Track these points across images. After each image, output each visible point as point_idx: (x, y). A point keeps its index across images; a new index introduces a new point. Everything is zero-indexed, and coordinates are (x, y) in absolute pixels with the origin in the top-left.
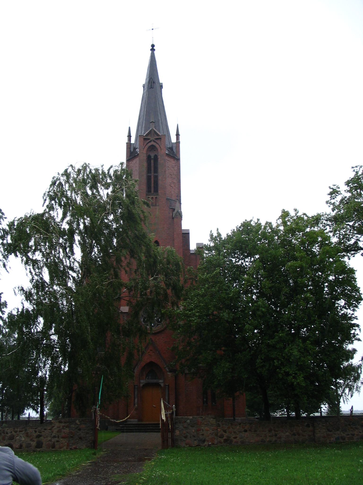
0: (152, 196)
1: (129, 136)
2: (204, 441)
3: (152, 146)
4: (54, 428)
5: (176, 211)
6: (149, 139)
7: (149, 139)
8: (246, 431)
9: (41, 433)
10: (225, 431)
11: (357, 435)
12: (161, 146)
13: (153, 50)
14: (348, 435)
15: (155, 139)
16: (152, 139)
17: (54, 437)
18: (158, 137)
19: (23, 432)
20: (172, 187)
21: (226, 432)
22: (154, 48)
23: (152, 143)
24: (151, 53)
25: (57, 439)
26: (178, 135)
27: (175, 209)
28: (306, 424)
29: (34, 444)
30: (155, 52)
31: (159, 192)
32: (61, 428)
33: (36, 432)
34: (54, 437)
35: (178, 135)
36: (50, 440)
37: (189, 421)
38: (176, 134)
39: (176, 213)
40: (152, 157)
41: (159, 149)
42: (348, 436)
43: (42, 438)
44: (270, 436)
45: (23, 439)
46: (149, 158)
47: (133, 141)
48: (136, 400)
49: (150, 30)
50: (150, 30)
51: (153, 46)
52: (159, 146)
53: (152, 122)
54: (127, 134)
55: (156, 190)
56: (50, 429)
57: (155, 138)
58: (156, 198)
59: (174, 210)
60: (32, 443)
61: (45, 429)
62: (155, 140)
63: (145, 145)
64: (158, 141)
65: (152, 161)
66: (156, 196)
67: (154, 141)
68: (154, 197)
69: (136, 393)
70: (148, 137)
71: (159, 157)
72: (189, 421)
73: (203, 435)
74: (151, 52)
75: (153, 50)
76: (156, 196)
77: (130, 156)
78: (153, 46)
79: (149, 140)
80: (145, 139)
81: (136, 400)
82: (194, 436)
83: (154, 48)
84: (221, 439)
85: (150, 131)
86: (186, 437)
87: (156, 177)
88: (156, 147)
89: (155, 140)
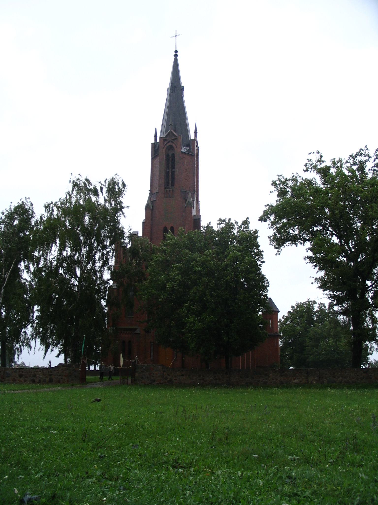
0: (169, 189)
1: (156, 136)
2: (154, 381)
3: (170, 145)
4: (60, 370)
5: (188, 201)
6: (168, 140)
7: (168, 140)
8: (183, 375)
9: (52, 373)
10: (168, 375)
11: (262, 381)
12: (177, 146)
13: (176, 56)
14: (255, 381)
15: (172, 140)
16: (170, 139)
17: (60, 375)
18: (175, 138)
19: (41, 372)
20: (186, 180)
21: (169, 376)
22: (177, 54)
23: (171, 143)
24: (175, 58)
25: (61, 377)
26: (196, 133)
27: (187, 199)
28: (225, 372)
29: (48, 380)
30: (178, 57)
31: (175, 185)
32: (64, 370)
33: (49, 372)
34: (60, 375)
35: (196, 133)
36: (57, 378)
37: (144, 367)
38: (194, 132)
39: (188, 203)
40: (170, 156)
41: (175, 149)
42: (255, 382)
43: (52, 376)
44: (199, 380)
45: (41, 376)
46: (168, 156)
47: (158, 141)
48: (152, 354)
49: (173, 37)
50: (173, 37)
51: (176, 52)
52: (176, 145)
53: (171, 125)
54: (154, 135)
55: (173, 184)
56: (58, 371)
57: (172, 139)
58: (173, 190)
59: (186, 200)
60: (46, 379)
61: (54, 371)
62: (172, 140)
63: (164, 146)
64: (175, 142)
65: (170, 159)
66: (172, 189)
67: (172, 142)
68: (171, 190)
69: (152, 348)
70: (167, 139)
71: (176, 155)
72: (144, 367)
73: (153, 377)
74: (174, 57)
75: (176, 56)
76: (172, 189)
77: (155, 154)
78: (176, 52)
79: (168, 141)
80: (164, 140)
81: (152, 354)
82: (148, 378)
83: (177, 54)
84: (165, 380)
85: (169, 133)
86: (142, 378)
87: (173, 173)
88: (173, 147)
89: (172, 140)
